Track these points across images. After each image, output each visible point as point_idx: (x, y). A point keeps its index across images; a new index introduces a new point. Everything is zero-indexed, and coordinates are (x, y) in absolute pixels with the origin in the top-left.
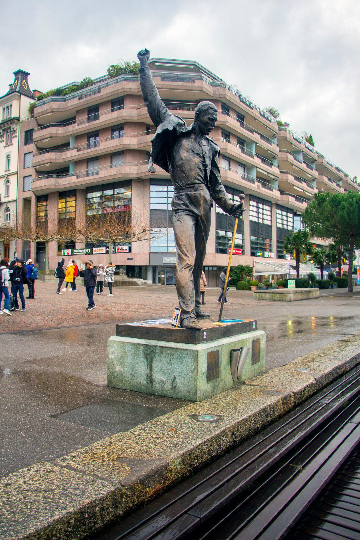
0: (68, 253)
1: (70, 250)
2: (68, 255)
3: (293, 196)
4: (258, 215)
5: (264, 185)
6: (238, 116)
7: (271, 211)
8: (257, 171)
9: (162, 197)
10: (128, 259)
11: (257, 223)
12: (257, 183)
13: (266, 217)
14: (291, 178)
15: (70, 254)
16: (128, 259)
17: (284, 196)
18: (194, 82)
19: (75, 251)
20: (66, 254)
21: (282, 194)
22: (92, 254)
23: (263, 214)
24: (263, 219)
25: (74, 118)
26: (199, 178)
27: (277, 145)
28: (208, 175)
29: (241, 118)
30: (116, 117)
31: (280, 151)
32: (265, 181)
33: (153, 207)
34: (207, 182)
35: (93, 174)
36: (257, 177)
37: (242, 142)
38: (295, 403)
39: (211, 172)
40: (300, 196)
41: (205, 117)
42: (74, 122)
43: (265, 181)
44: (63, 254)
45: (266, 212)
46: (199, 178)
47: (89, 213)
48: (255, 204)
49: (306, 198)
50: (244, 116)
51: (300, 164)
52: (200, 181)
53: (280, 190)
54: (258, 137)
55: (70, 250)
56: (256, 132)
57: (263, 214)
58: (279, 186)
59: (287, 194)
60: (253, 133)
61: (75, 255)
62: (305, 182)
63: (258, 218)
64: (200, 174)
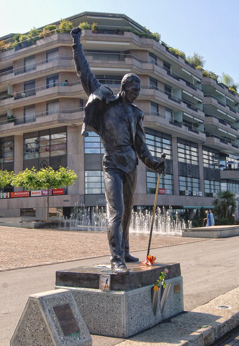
0: (7, 196)
1: (9, 193)
2: (7, 198)
3: (218, 137)
4: (185, 156)
5: (190, 129)
6: (164, 65)
7: (197, 152)
8: (183, 115)
9: (95, 144)
10: (65, 201)
11: (185, 164)
12: (184, 127)
13: (193, 158)
14: (216, 121)
15: (9, 197)
16: (65, 201)
17: (210, 138)
18: (123, 34)
19: (12, 193)
20: (5, 197)
21: (207, 136)
22: (30, 196)
23: (190, 155)
24: (191, 160)
25: (11, 68)
26: (127, 141)
27: (202, 91)
28: (134, 138)
29: (167, 66)
30: (51, 67)
31: (205, 96)
32: (190, 124)
33: (88, 151)
34: (133, 144)
35: (30, 121)
36: (184, 120)
37: (168, 90)
38: (215, 338)
39: (136, 134)
40: (225, 137)
41: (130, 87)
42: (12, 72)
43: (190, 124)
44: (1, 197)
45: (193, 153)
46: (127, 141)
47: (27, 157)
48: (182, 146)
49: (230, 139)
50: (170, 64)
51: (223, 107)
52: (127, 143)
53: (205, 132)
54: (184, 83)
55: (9, 193)
56: (181, 79)
57: (190, 155)
58: (204, 129)
59: (212, 136)
60: (179, 80)
61: (13, 198)
62: (229, 124)
63: (185, 159)
64: (127, 137)
